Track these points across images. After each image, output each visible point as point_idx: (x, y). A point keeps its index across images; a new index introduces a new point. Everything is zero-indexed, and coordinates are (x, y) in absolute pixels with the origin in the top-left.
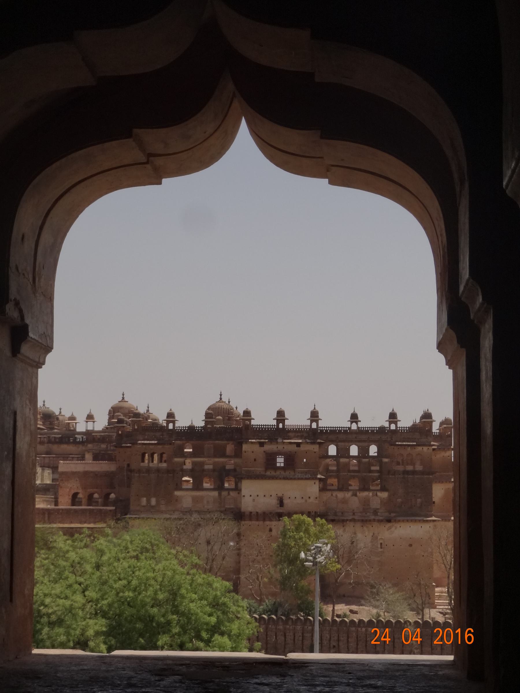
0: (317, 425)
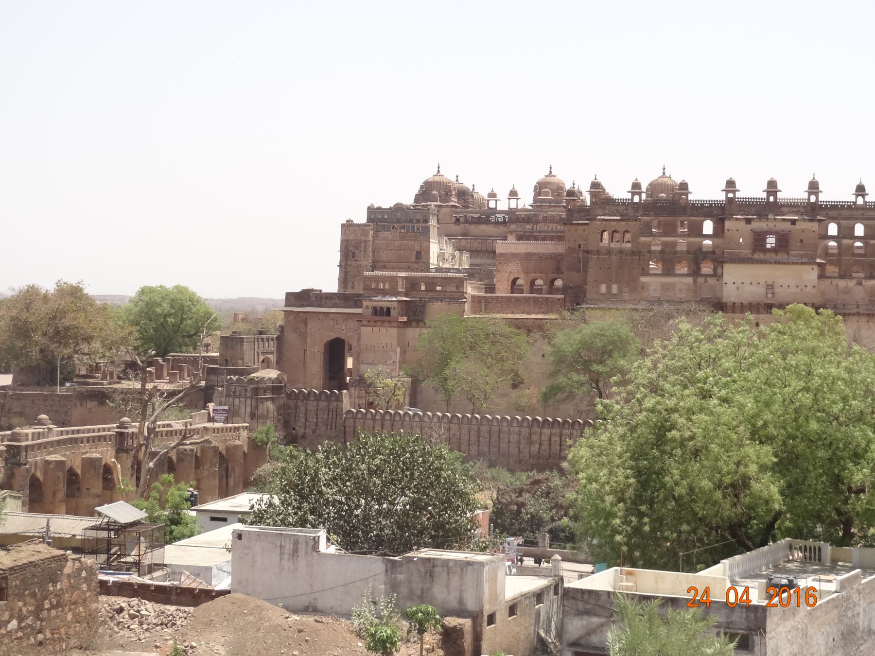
0: (817, 198)
